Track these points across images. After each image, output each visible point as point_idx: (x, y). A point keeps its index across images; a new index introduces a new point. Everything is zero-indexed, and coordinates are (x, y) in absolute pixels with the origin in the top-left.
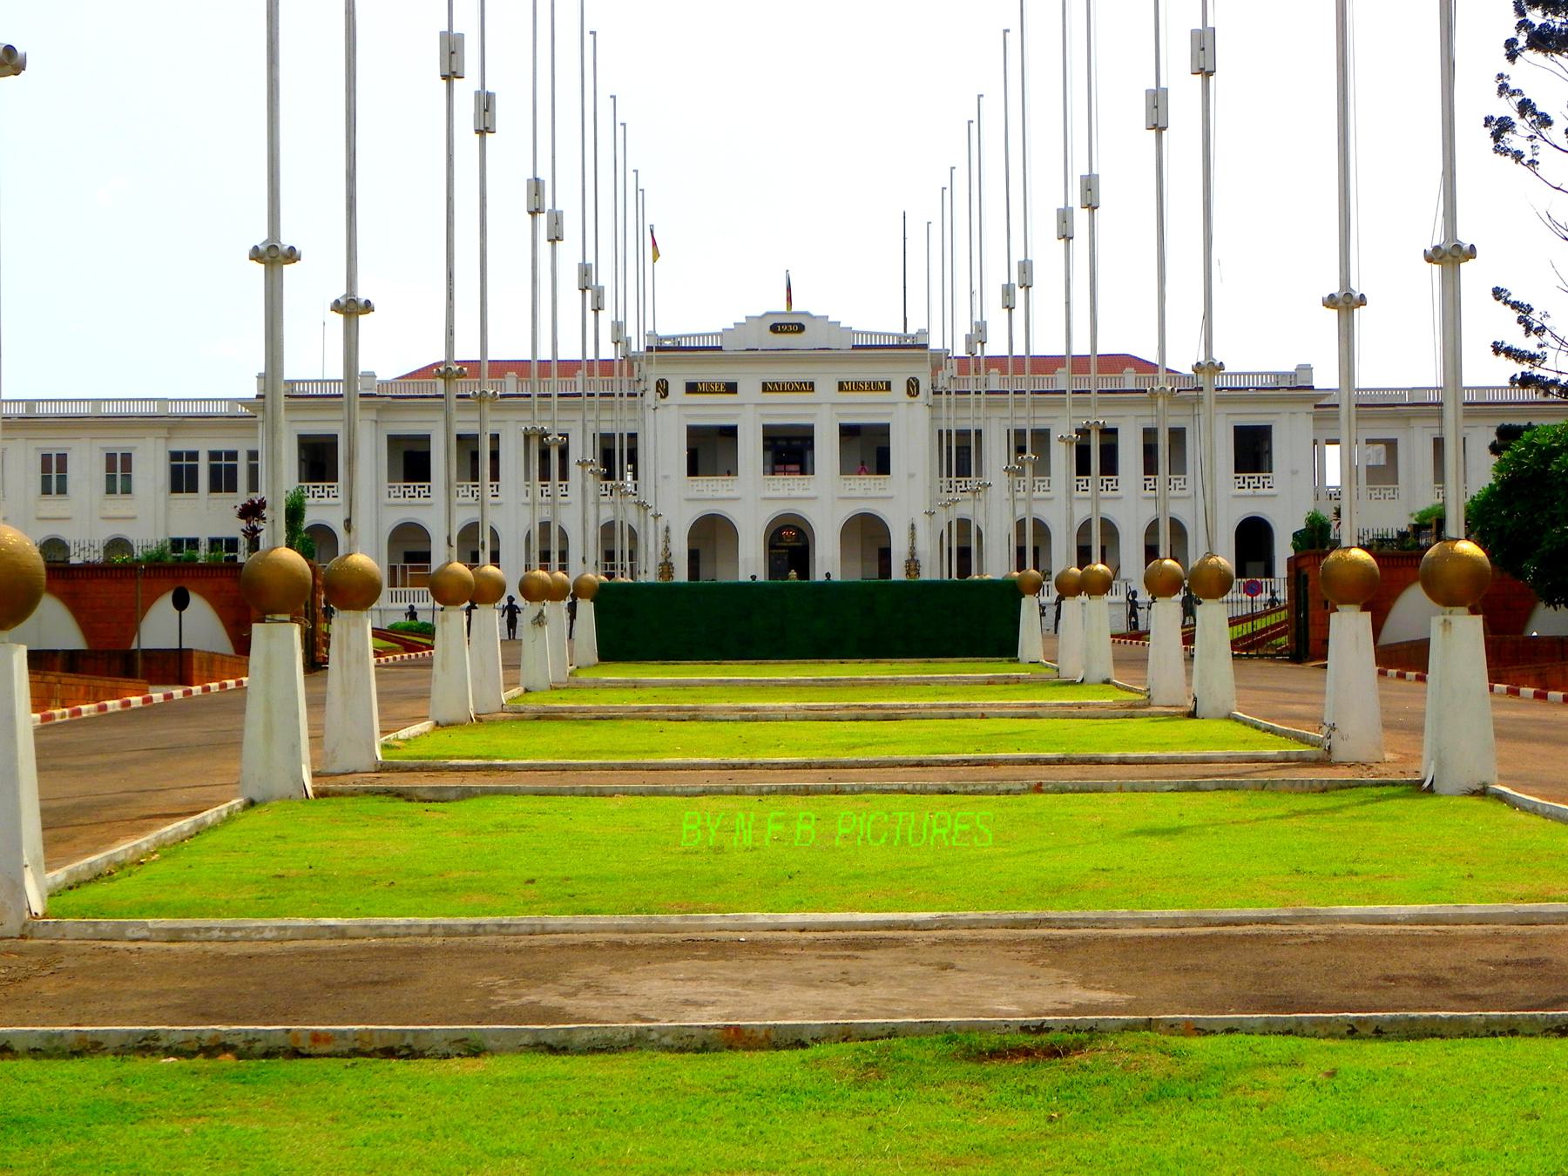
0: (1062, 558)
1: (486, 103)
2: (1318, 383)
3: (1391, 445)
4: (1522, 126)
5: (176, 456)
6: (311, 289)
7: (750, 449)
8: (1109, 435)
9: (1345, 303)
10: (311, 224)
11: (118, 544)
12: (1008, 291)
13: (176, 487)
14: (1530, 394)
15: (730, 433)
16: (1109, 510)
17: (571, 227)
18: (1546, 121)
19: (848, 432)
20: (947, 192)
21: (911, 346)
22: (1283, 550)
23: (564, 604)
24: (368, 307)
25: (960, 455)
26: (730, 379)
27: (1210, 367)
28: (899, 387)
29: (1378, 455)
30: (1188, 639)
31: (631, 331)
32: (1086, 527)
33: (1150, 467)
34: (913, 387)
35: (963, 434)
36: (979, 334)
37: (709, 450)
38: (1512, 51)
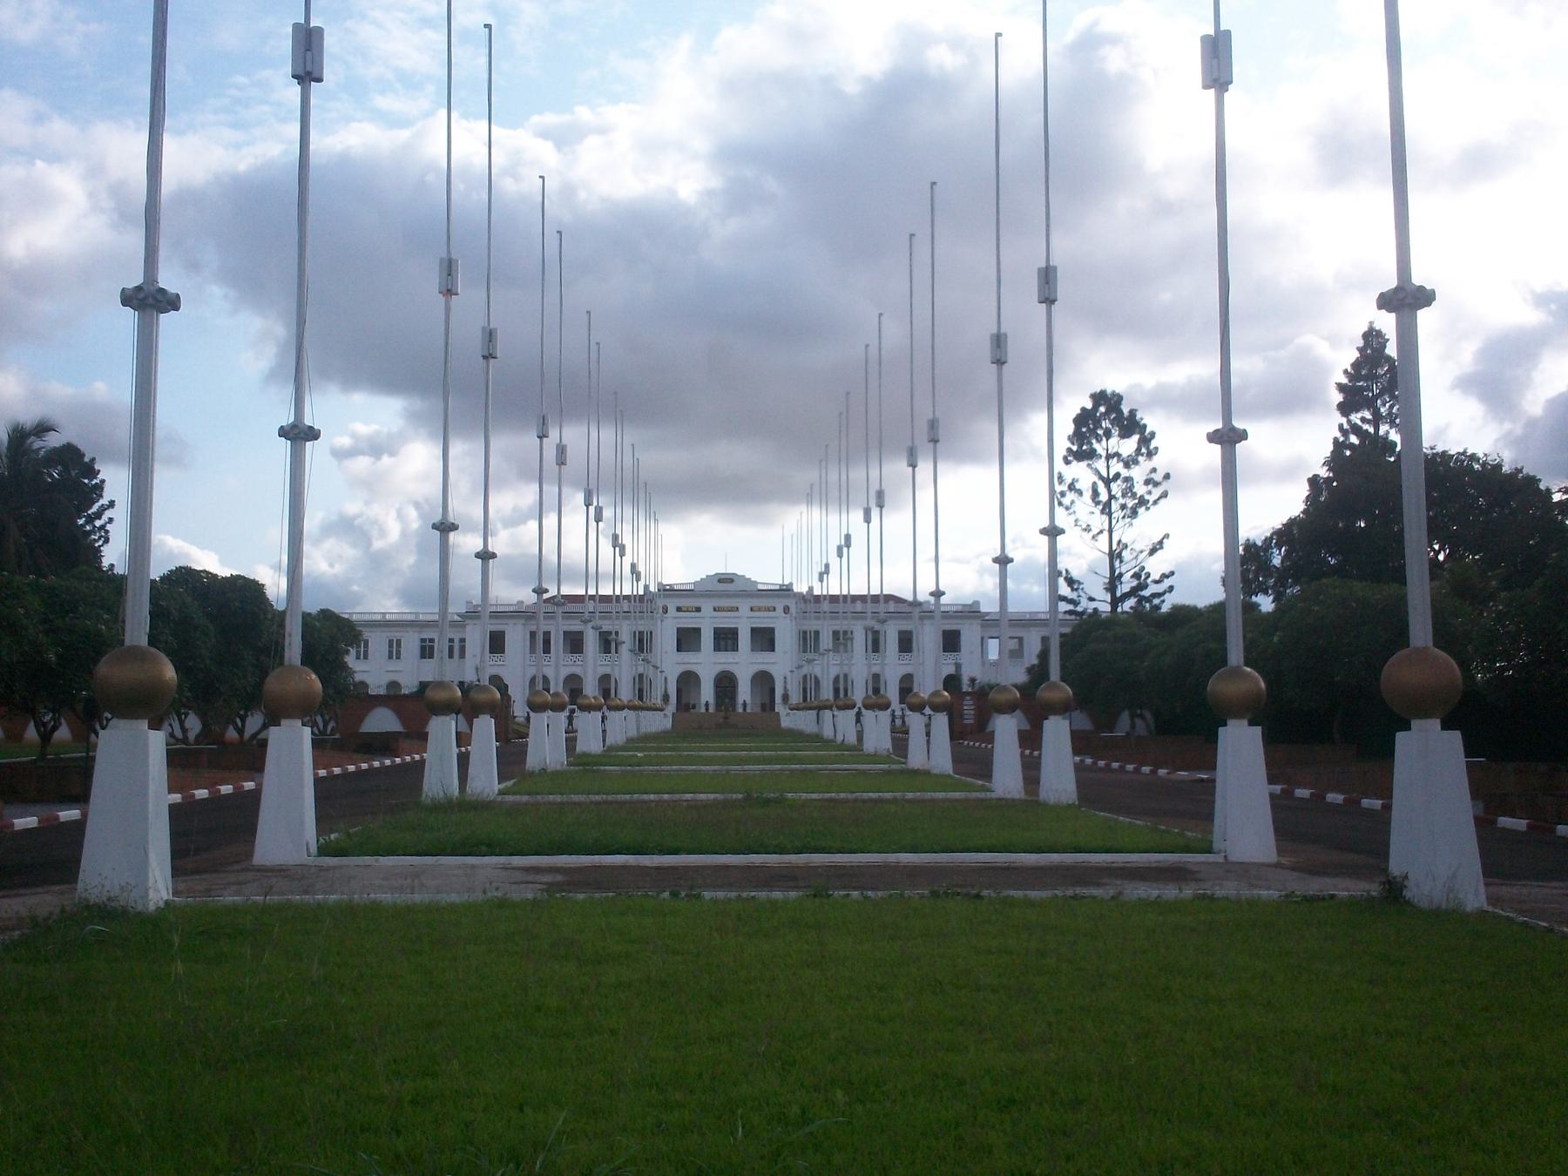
3: (1021, 639)
5: (423, 640)
7: (707, 639)
8: (547, 635)
11: (394, 685)
12: (840, 549)
13: (423, 656)
15: (698, 631)
16: (817, 671)
18: (1080, 493)
19: (755, 631)
21: (785, 591)
25: (808, 641)
26: (697, 605)
27: (938, 594)
28: (780, 609)
29: (1013, 644)
34: (786, 610)
36: (811, 589)
37: (687, 639)
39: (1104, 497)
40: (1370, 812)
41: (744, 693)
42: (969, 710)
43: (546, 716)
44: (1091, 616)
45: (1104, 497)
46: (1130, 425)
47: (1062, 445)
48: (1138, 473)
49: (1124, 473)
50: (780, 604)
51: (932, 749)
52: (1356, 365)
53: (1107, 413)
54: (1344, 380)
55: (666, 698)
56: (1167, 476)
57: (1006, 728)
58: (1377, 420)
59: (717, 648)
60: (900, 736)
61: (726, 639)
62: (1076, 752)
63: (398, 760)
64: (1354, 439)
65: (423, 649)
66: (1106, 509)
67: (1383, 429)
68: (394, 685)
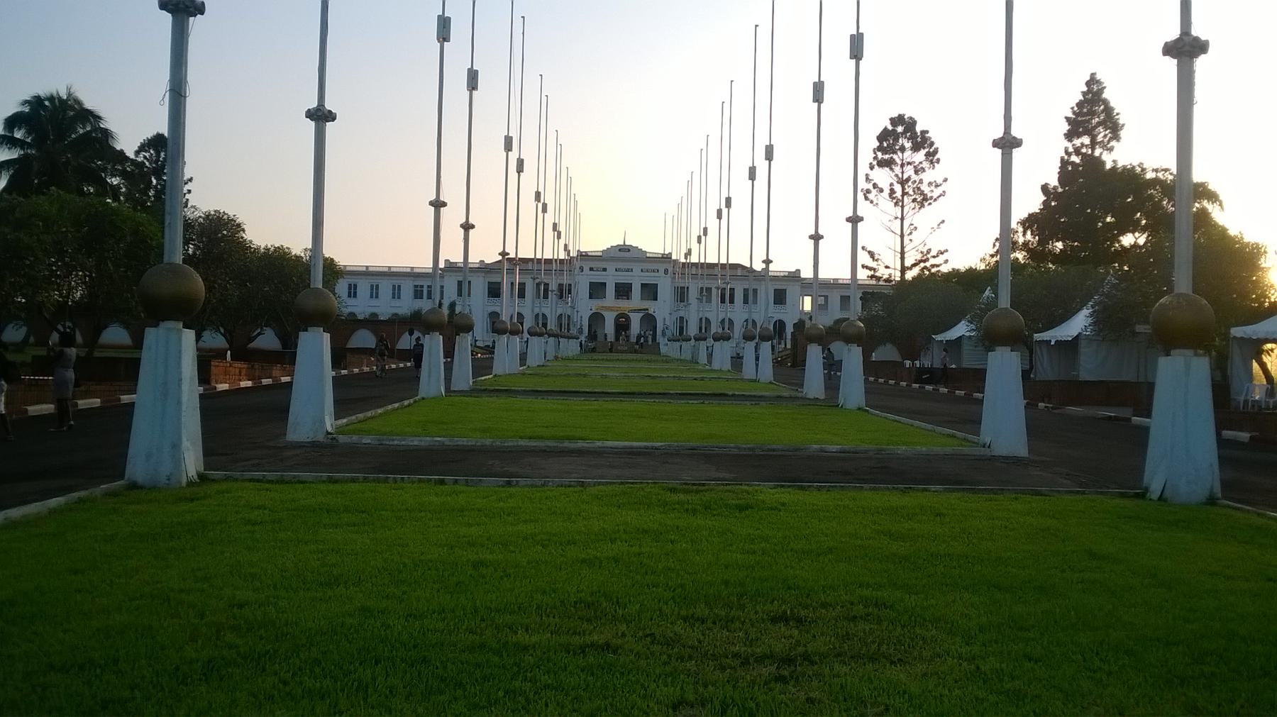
0: (714, 329)
1: (520, 163)
3: (826, 297)
4: (874, 192)
6: (452, 218)
7: (610, 290)
9: (816, 238)
10: (453, 194)
11: (396, 314)
12: (699, 238)
13: (416, 297)
16: (547, 312)
17: (550, 208)
18: (881, 191)
20: (680, 205)
21: (666, 258)
22: (789, 330)
25: (681, 294)
28: (662, 272)
29: (821, 300)
30: (757, 359)
31: (571, 248)
33: (746, 301)
34: (666, 271)
36: (689, 253)
37: (597, 290)
38: (872, 168)
39: (899, 194)
40: (977, 399)
41: (635, 328)
42: (792, 345)
43: (535, 339)
44: (886, 281)
45: (899, 194)
46: (921, 141)
47: (866, 156)
48: (928, 176)
49: (914, 177)
50: (662, 268)
51: (761, 366)
52: (1080, 105)
54: (1070, 115)
55: (581, 331)
56: (945, 180)
57: (814, 354)
58: (1093, 144)
60: (737, 360)
61: (623, 291)
62: (1145, 430)
63: (344, 372)
64: (1076, 159)
65: (416, 291)
66: (899, 203)
67: (1097, 153)
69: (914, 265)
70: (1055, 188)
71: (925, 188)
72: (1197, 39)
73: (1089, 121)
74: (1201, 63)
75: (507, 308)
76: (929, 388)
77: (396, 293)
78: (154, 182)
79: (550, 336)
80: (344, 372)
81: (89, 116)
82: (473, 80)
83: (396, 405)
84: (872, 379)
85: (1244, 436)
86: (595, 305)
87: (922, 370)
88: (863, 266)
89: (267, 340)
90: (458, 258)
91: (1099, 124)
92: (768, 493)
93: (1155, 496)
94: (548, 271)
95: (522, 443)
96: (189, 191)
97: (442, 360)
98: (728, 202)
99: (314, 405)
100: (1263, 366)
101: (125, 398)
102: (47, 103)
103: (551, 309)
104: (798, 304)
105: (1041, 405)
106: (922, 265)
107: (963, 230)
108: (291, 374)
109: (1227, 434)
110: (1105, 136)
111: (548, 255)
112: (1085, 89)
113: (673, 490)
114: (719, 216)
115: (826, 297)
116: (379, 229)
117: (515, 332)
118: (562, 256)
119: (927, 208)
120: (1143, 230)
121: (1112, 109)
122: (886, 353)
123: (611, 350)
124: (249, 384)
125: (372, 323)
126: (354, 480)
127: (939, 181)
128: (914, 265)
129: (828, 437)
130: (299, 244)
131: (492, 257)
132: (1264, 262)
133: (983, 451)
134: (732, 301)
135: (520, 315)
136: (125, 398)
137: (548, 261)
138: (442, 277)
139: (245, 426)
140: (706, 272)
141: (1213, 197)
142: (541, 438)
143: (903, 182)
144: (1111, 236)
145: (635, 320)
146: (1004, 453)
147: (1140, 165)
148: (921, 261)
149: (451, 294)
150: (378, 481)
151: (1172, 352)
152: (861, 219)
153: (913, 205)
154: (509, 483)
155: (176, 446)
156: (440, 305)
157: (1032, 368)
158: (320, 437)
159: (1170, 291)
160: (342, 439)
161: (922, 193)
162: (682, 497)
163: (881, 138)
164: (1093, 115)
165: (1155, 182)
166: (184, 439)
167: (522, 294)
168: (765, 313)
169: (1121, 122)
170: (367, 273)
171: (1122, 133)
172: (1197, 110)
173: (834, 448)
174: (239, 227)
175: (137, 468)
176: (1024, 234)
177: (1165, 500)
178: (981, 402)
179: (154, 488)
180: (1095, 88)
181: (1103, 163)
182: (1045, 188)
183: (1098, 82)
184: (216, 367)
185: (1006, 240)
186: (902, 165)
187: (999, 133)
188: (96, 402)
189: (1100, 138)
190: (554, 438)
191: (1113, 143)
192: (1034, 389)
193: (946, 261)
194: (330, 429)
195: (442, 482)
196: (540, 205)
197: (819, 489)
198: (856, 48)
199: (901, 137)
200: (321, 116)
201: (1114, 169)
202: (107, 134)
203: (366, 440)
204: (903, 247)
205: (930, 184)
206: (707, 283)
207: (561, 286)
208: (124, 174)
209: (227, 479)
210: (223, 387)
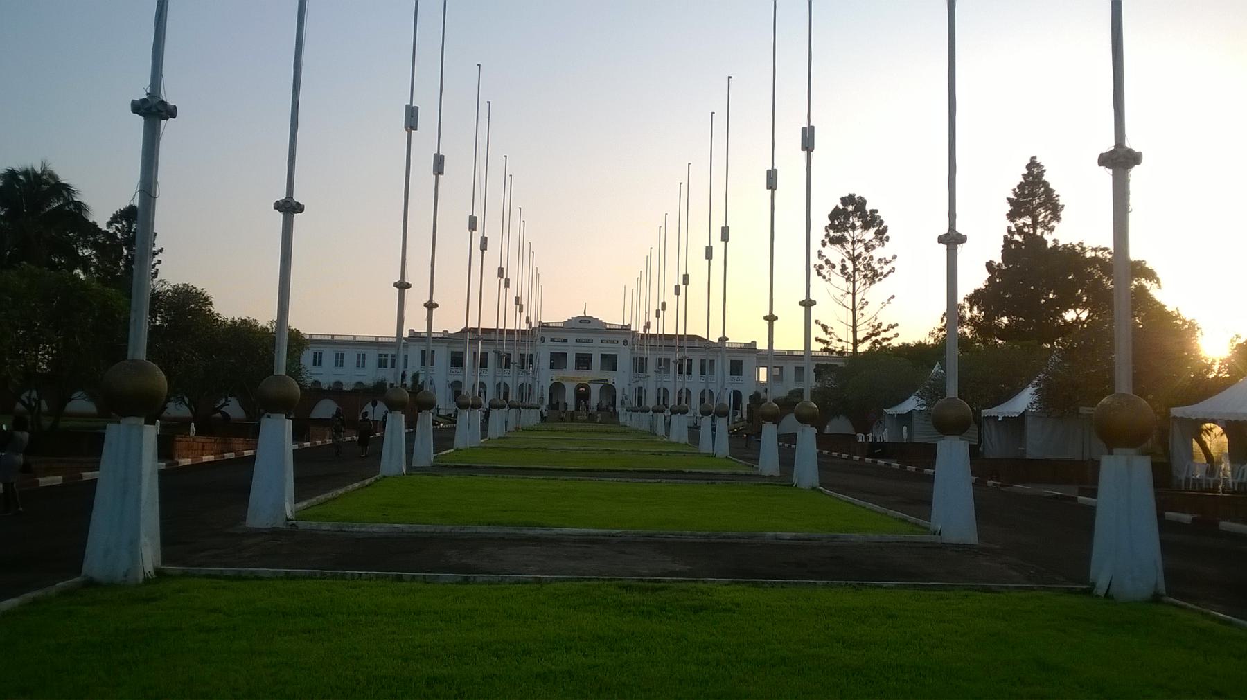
0: (672, 401)
1: (484, 242)
2: (758, 347)
3: (781, 368)
4: (826, 268)
7: (571, 360)
9: (771, 319)
11: (359, 383)
12: (658, 312)
14: (827, 354)
16: (508, 381)
18: (834, 267)
20: (639, 280)
21: (626, 329)
22: (745, 401)
23: (479, 414)
24: (436, 306)
25: (640, 365)
27: (723, 339)
28: (621, 343)
29: (776, 371)
30: (714, 429)
31: (532, 320)
32: (681, 391)
33: (703, 372)
34: (625, 342)
35: (641, 359)
36: (648, 326)
37: (558, 360)
38: (824, 244)
39: (850, 270)
41: (595, 398)
42: (750, 418)
44: (839, 353)
46: (872, 221)
47: (818, 233)
48: (878, 253)
49: (865, 254)
50: (621, 339)
51: (717, 441)
52: (1021, 186)
53: (854, 212)
54: (1012, 196)
55: (541, 400)
56: (895, 257)
58: (1035, 224)
59: (578, 368)
60: (694, 430)
61: (583, 361)
62: (1091, 511)
63: (307, 444)
64: (1017, 237)
66: (850, 278)
68: (338, 383)
69: (866, 339)
70: (999, 265)
71: (877, 266)
72: (1130, 151)
73: (1030, 203)
74: (1135, 174)
75: (469, 377)
76: (881, 462)
77: (361, 361)
78: (125, 252)
79: (511, 407)
80: (307, 444)
81: (61, 189)
82: (439, 165)
83: (357, 485)
84: (825, 452)
85: (1186, 518)
86: (557, 375)
87: (874, 445)
88: (817, 340)
89: (234, 409)
90: (422, 328)
91: (1040, 205)
92: (724, 591)
93: (1101, 592)
94: (510, 342)
95: (481, 529)
96: (159, 262)
97: (404, 431)
98: (686, 279)
99: (275, 495)
100: (1203, 445)
101: (87, 475)
102: (21, 177)
103: (512, 378)
104: (754, 374)
105: (990, 482)
106: (874, 338)
107: (912, 308)
108: (255, 447)
109: (1170, 515)
110: (1046, 217)
111: (510, 326)
112: (1026, 172)
113: (629, 588)
114: (677, 292)
115: (781, 368)
116: (345, 298)
117: (476, 406)
118: (524, 327)
119: (878, 285)
120: (1084, 307)
121: (1052, 191)
122: (839, 425)
123: (572, 420)
124: (211, 458)
125: (336, 392)
126: (311, 577)
127: (889, 258)
128: (866, 339)
129: (781, 523)
130: (265, 317)
131: (455, 327)
132: (1198, 334)
133: (932, 538)
134: (689, 372)
135: (482, 385)
136: (87, 475)
137: (510, 332)
138: (405, 346)
139: (201, 508)
140: (665, 343)
141: (1150, 275)
142: (501, 524)
143: (854, 259)
144: (1055, 313)
145: (595, 390)
146: (954, 539)
147: (1080, 244)
148: (872, 335)
149: (414, 365)
150: (334, 577)
151: (1115, 450)
152: (814, 303)
153: (863, 281)
154: (466, 581)
155: (134, 543)
156: (404, 375)
157: (980, 441)
158: (280, 524)
159: (1112, 392)
160: (302, 525)
161: (873, 270)
162: (637, 597)
163: (835, 214)
164: (1033, 196)
165: (1095, 260)
166: (142, 535)
167: (484, 364)
168: (722, 385)
169: (1061, 203)
170: (332, 342)
171: (1062, 214)
172: (1134, 220)
173: (788, 535)
174: (207, 301)
175: (95, 563)
176: (971, 310)
177: (1112, 597)
178: (931, 479)
179: (111, 586)
180: (1035, 171)
181: (1045, 242)
182: (989, 266)
183: (1039, 165)
184: (181, 442)
185: (953, 315)
186: (853, 243)
187: (944, 230)
188: (58, 479)
189: (1041, 218)
190: (512, 524)
191: (1054, 223)
192: (978, 461)
193: (897, 335)
194: (289, 515)
195: (399, 579)
196: (503, 281)
197: (773, 585)
198: (808, 140)
199: (852, 216)
200: (289, 208)
201: (1055, 247)
202: (80, 207)
203: (326, 526)
204: (854, 321)
205: (880, 260)
206: (664, 355)
207: (522, 355)
208: (95, 245)
209: (184, 575)
210: (186, 461)
